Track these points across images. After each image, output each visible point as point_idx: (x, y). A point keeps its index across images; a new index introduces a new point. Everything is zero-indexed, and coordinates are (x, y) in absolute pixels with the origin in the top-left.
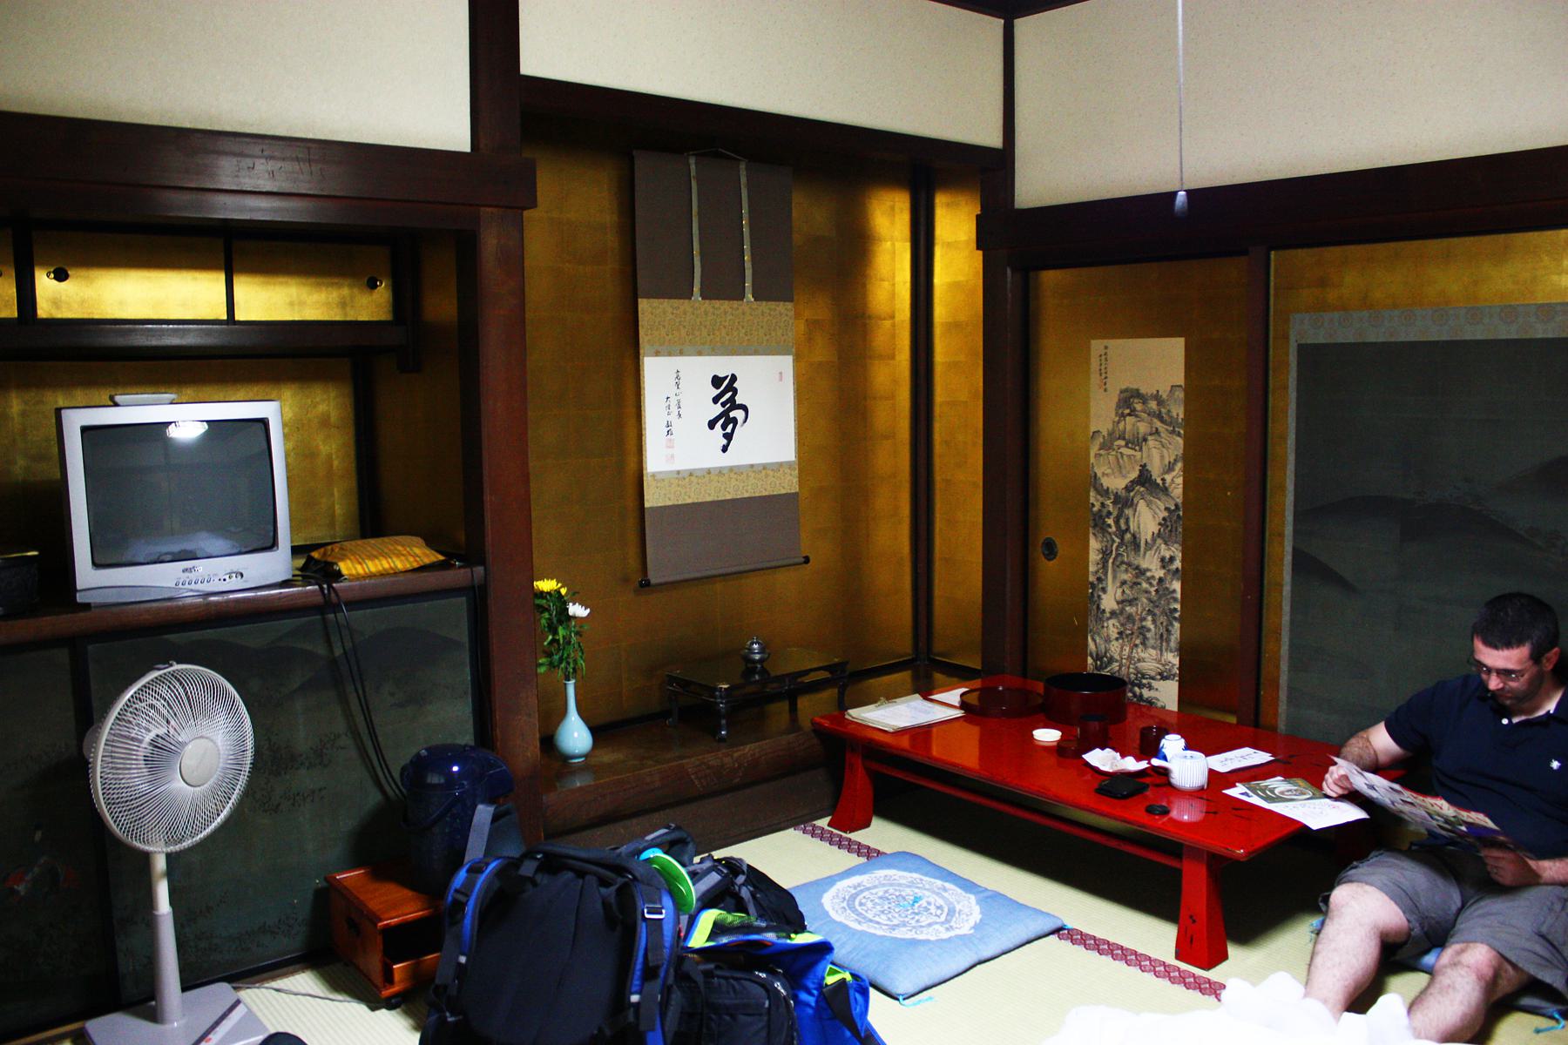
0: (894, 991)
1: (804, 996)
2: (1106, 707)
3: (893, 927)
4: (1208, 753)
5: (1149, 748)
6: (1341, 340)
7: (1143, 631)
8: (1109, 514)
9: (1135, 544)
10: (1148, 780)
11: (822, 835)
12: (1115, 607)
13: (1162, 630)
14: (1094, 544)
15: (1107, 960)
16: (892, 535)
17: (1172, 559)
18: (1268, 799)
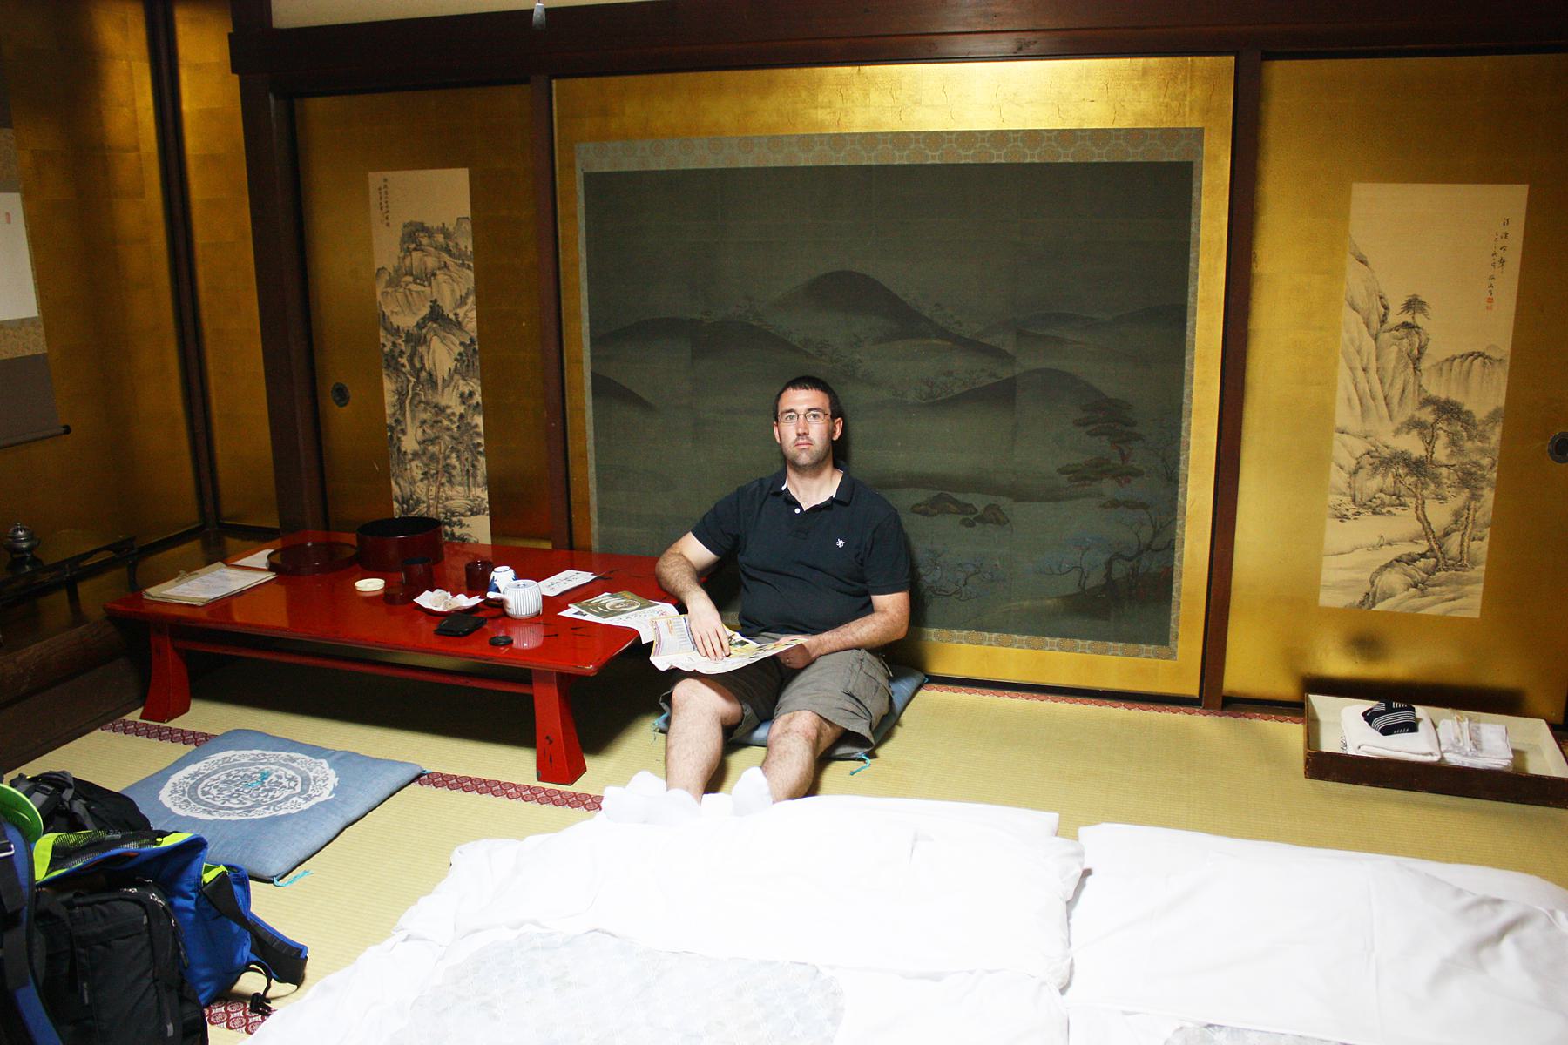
0: (266, 874)
1: (180, 902)
2: (419, 548)
3: (249, 810)
4: (539, 577)
5: (478, 581)
6: (625, 169)
7: (448, 469)
8: (402, 352)
9: (432, 382)
10: (482, 614)
11: (136, 730)
12: (416, 447)
13: (468, 466)
14: (389, 386)
15: (488, 798)
16: (160, 392)
17: (471, 394)
18: (601, 614)
